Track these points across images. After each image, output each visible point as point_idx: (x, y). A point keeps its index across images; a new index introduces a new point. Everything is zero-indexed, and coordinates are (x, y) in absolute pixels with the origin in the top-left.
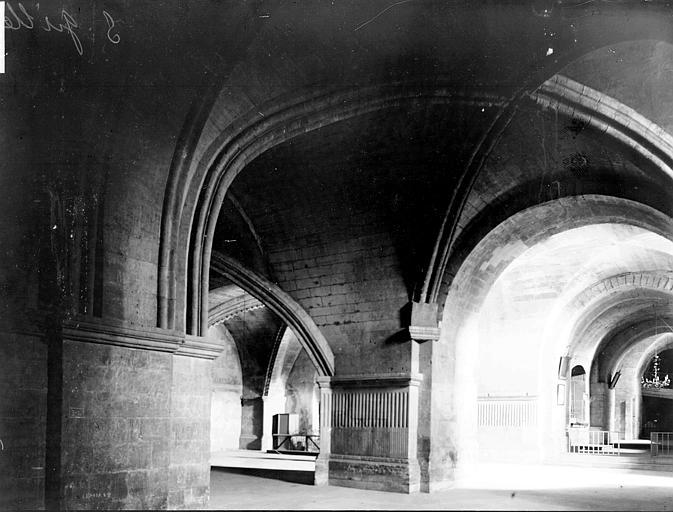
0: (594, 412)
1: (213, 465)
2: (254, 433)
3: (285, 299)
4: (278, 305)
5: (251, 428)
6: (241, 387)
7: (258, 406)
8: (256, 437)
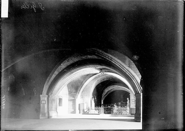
0: (138, 121)
1: (79, 113)
2: (73, 109)
3: (132, 72)
4: (130, 74)
5: (72, 107)
6: (68, 96)
7: (74, 101)
8: (74, 110)
